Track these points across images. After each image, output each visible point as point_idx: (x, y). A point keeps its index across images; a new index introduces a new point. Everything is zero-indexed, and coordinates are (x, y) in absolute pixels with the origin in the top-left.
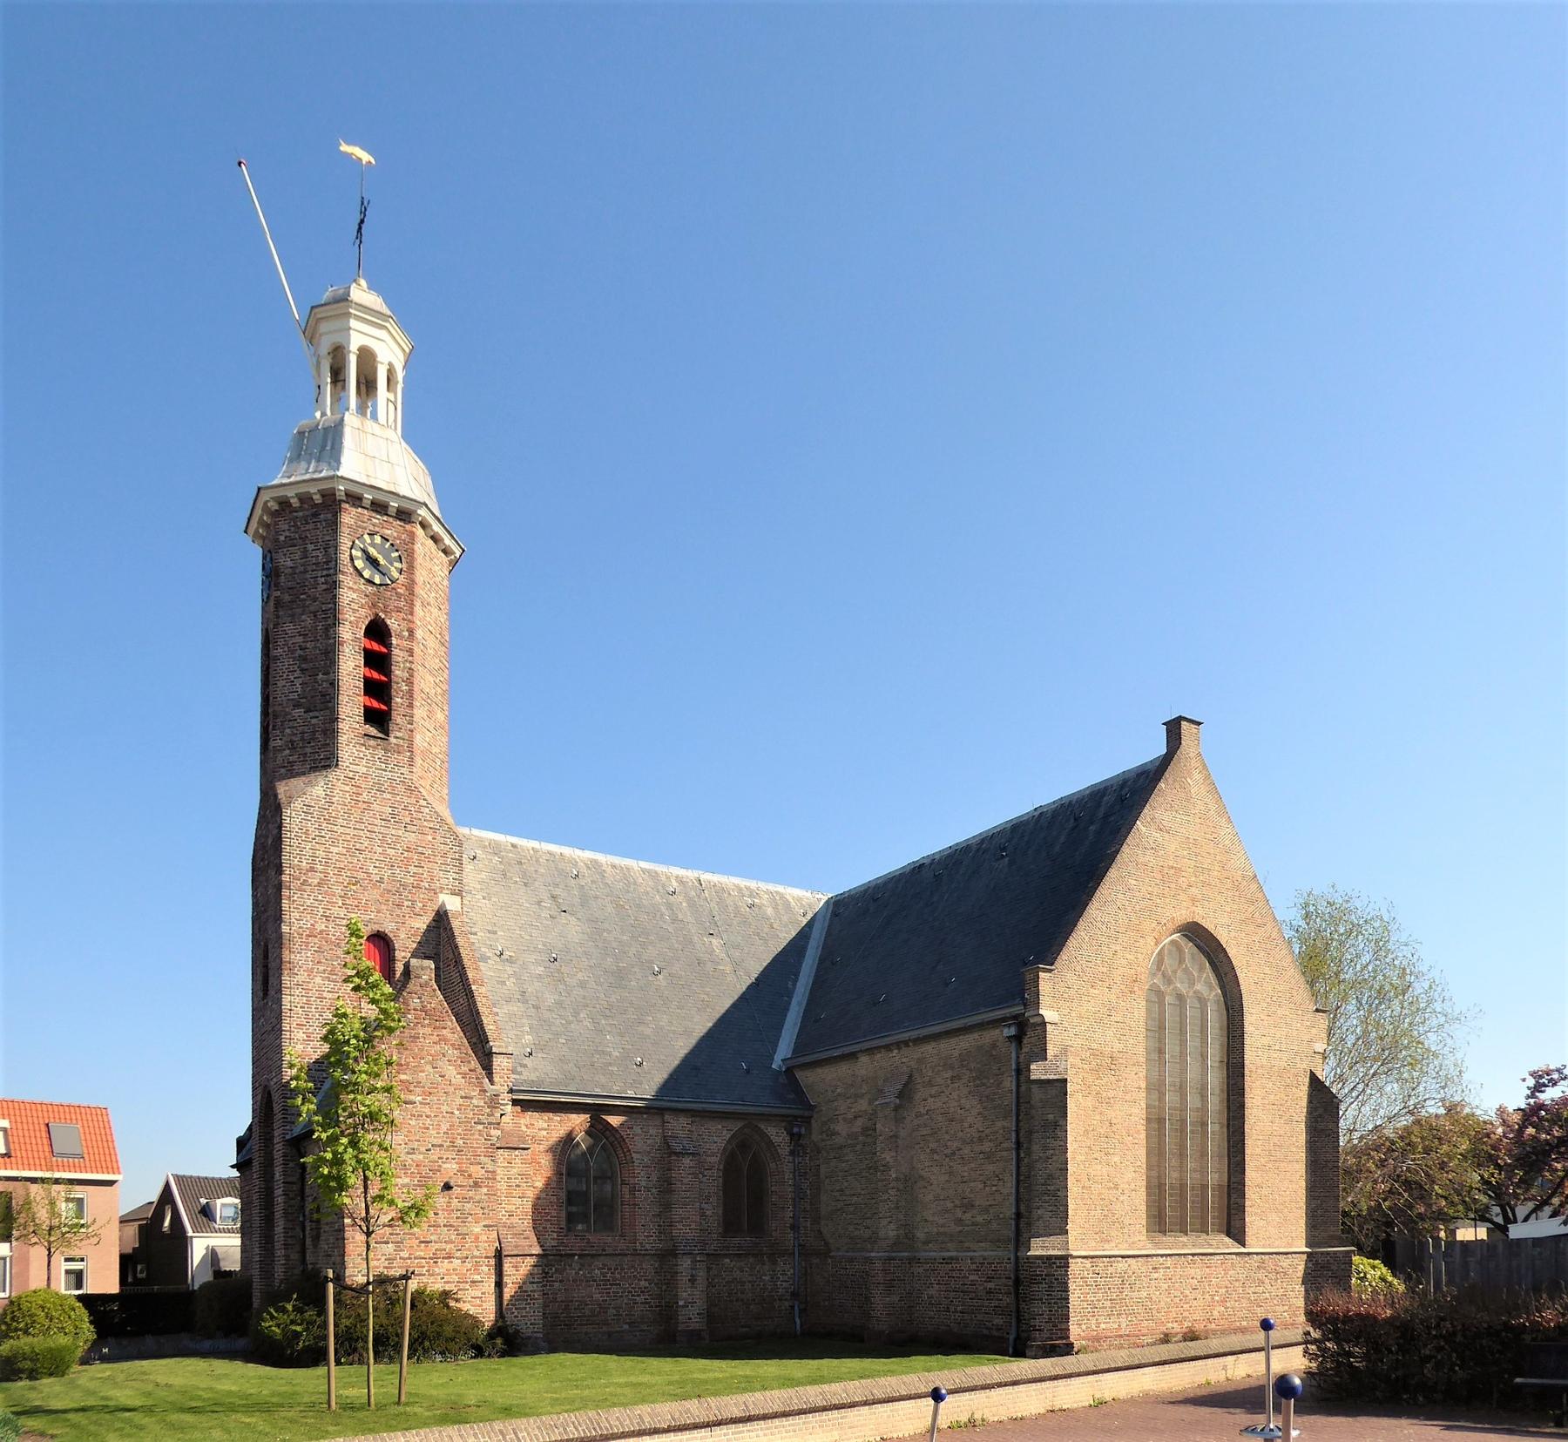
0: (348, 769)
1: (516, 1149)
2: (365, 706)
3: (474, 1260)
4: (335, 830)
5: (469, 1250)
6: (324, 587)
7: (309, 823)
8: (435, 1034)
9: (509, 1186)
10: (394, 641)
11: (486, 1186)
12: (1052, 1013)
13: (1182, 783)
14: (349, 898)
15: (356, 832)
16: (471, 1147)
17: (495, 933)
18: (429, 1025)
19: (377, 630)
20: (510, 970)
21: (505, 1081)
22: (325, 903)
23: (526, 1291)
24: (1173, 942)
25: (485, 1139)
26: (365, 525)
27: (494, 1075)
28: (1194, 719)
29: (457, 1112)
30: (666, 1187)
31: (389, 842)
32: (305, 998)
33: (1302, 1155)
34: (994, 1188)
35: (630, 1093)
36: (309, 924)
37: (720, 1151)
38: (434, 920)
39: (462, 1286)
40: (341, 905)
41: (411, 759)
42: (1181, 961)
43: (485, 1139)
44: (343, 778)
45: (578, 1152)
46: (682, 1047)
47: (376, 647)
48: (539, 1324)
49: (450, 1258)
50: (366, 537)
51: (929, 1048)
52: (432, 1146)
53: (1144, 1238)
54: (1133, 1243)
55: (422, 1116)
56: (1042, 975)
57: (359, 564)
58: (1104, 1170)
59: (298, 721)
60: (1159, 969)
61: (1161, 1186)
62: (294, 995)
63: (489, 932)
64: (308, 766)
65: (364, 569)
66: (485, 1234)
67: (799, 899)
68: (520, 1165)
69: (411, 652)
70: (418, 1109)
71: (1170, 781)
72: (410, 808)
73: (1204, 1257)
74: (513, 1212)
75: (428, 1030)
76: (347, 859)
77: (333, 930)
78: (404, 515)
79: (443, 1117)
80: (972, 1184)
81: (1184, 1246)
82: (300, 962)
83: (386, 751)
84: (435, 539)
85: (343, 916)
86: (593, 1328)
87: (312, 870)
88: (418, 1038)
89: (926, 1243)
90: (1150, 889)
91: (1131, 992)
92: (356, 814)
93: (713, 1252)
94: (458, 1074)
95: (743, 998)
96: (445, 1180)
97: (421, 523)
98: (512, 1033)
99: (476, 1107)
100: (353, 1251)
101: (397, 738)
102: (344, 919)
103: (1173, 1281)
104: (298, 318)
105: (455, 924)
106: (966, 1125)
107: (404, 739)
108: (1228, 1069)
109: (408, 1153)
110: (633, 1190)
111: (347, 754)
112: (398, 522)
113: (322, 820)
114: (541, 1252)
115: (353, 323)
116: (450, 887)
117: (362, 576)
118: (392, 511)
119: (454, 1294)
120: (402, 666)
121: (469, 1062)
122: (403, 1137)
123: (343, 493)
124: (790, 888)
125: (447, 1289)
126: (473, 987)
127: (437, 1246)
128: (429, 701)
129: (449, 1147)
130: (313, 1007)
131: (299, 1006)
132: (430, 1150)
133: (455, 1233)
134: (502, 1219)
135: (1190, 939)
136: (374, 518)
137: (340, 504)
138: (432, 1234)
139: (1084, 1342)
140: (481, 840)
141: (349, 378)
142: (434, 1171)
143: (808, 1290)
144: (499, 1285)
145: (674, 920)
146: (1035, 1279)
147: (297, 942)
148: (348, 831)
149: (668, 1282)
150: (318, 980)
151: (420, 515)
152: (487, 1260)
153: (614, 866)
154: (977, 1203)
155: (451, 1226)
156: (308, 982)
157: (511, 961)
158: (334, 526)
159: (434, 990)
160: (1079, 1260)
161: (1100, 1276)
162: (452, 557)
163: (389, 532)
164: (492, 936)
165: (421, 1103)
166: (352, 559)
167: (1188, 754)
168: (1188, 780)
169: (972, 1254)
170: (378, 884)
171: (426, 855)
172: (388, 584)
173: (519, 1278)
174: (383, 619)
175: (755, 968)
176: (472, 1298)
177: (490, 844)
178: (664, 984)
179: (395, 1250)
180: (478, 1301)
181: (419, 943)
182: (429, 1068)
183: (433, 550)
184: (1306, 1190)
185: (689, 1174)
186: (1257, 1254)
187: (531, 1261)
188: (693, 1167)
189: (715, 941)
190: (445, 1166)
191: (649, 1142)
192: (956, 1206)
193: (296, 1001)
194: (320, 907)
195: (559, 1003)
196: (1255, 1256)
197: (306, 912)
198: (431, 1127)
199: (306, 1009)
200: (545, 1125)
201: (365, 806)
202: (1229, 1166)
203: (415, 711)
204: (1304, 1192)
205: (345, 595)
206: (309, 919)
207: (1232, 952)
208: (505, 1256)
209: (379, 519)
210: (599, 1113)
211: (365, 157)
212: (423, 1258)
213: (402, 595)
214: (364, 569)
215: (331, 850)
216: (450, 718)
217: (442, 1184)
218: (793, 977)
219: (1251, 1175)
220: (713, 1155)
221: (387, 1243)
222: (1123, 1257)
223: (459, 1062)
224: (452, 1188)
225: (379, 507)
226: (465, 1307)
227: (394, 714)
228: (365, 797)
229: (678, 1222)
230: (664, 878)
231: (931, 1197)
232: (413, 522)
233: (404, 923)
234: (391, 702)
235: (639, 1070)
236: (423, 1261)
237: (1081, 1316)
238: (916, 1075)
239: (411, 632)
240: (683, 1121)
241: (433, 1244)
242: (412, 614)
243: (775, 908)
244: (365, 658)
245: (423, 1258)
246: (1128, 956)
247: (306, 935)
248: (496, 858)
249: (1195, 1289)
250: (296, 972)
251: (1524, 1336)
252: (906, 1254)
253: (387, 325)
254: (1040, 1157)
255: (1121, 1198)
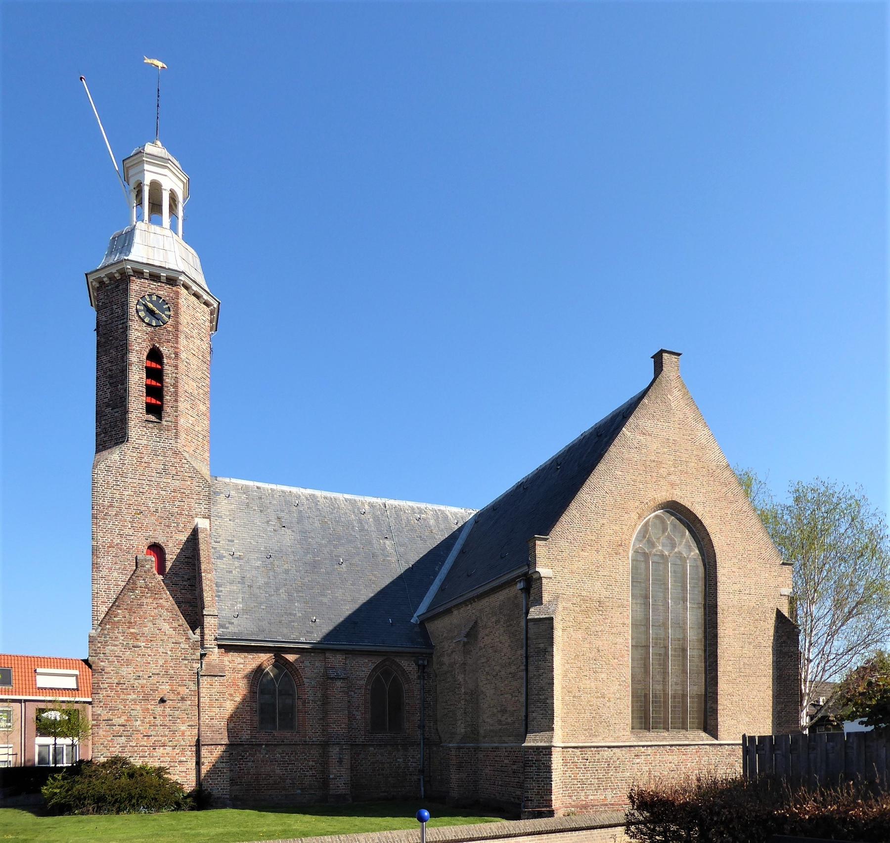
0: (135, 442)
1: (217, 676)
2: (146, 403)
3: (181, 748)
4: (127, 481)
5: (178, 741)
6: (121, 330)
7: (109, 477)
8: (155, 602)
9: (211, 700)
10: (165, 361)
11: (190, 700)
12: (547, 570)
13: (663, 399)
14: (135, 523)
15: (140, 481)
16: (179, 675)
17: (233, 541)
18: (151, 597)
19: (155, 355)
20: (237, 564)
21: (212, 633)
22: (120, 526)
23: (217, 768)
24: (657, 516)
25: (189, 670)
26: (146, 289)
27: (205, 629)
28: (674, 351)
29: (169, 653)
30: (325, 701)
31: (162, 487)
32: (106, 586)
33: (770, 671)
34: (516, 698)
35: (303, 639)
36: (109, 539)
37: (367, 677)
38: (191, 535)
39: (172, 764)
40: (130, 527)
41: (177, 436)
42: (664, 530)
43: (189, 670)
44: (131, 448)
45: (269, 678)
46: (348, 609)
47: (154, 365)
48: (227, 789)
49: (164, 746)
50: (146, 297)
51: (485, 602)
52: (152, 674)
53: (628, 733)
54: (617, 737)
55: (145, 655)
56: (538, 542)
57: (142, 314)
58: (593, 684)
59: (108, 415)
60: (644, 537)
61: (646, 696)
62: (99, 584)
63: (229, 541)
64: (113, 443)
65: (145, 317)
66: (189, 731)
67: (455, 514)
68: (218, 686)
69: (176, 367)
70: (143, 651)
71: (653, 398)
72: (175, 465)
73: (680, 747)
74: (213, 716)
75: (151, 600)
76: (134, 498)
77: (125, 543)
78: (172, 281)
79: (160, 656)
80: (506, 696)
81: (664, 738)
82: (103, 563)
83: (160, 430)
84: (197, 296)
85: (131, 534)
86: (275, 792)
87: (111, 506)
88: (143, 605)
89: (484, 737)
90: (634, 477)
91: (616, 553)
92: (140, 470)
93: (362, 743)
94: (170, 628)
95: (400, 577)
96: (161, 696)
97: (183, 285)
98: (229, 603)
99: (183, 649)
100: (97, 742)
101: (167, 421)
102: (132, 536)
103: (653, 765)
104: (117, 169)
105: (201, 536)
106: (503, 654)
107: (172, 422)
108: (705, 609)
109: (136, 679)
110: (304, 703)
111: (134, 433)
112: (168, 286)
113: (118, 475)
114: (228, 743)
115: (146, 167)
116: (202, 513)
117: (144, 321)
118: (163, 279)
119: (167, 769)
120: (170, 376)
121: (178, 620)
122: (132, 669)
123: (131, 271)
124: (449, 507)
125: (162, 766)
126: (203, 574)
127: (155, 738)
128: (192, 398)
129: (164, 675)
130: (112, 591)
131: (103, 590)
132: (150, 677)
133: (168, 730)
134: (206, 721)
135: (672, 514)
136: (152, 284)
137: (129, 278)
138: (152, 731)
139: (573, 809)
140: (237, 485)
141: (144, 201)
142: (154, 691)
143: (431, 769)
144: (198, 763)
145: (362, 529)
146: (528, 764)
147: (102, 551)
148: (134, 481)
149: (324, 763)
150: (115, 574)
151: (182, 280)
152: (190, 748)
153: (325, 498)
154: (508, 709)
155: (165, 725)
156: (108, 576)
157: (239, 558)
158: (126, 291)
159: (154, 575)
160: (570, 750)
161: (588, 761)
162: (212, 307)
163: (162, 292)
164: (230, 543)
165: (144, 647)
166: (137, 311)
167: (668, 377)
168: (669, 396)
169: (506, 745)
170: (155, 513)
171: (187, 494)
172: (161, 326)
173: (213, 759)
174: (158, 348)
175: (414, 558)
176: (179, 772)
177: (242, 488)
178: (345, 570)
179: (126, 741)
180: (184, 774)
181: (181, 549)
182: (150, 624)
183: (195, 303)
184: (773, 697)
185: (340, 692)
186: (728, 745)
187: (221, 749)
188: (343, 687)
189: (387, 542)
190: (160, 687)
191: (315, 671)
192: (498, 712)
193: (101, 587)
194: (117, 529)
195: (266, 583)
196: (727, 746)
197: (107, 532)
198: (151, 662)
199: (107, 592)
200: (242, 661)
201: (146, 465)
202: (706, 681)
203: (179, 404)
204: (771, 699)
205: (133, 334)
206: (109, 536)
207: (706, 522)
208: (202, 745)
209: (155, 285)
210: (280, 653)
211: (160, 64)
212: (146, 746)
213: (170, 331)
214: (145, 317)
215: (124, 493)
216: (211, 409)
217: (159, 699)
218: (440, 563)
219: (723, 686)
220: (362, 679)
221: (121, 736)
222: (609, 747)
223: (171, 621)
224: (166, 701)
225: (155, 277)
226: (174, 778)
227: (165, 406)
228: (146, 459)
229: (332, 723)
230: (360, 504)
231: (486, 706)
232: (178, 285)
233: (172, 537)
234: (163, 399)
235: (313, 625)
236: (146, 748)
237: (572, 790)
238: (479, 621)
239: (176, 354)
240: (340, 657)
241: (153, 737)
242: (177, 343)
243: (437, 520)
244: (146, 373)
245: (146, 746)
246: (614, 528)
247: (107, 547)
248: (245, 496)
249: (672, 771)
250: (101, 569)
251: (786, 826)
252: (471, 745)
253: (168, 165)
254: (534, 675)
255: (608, 704)
